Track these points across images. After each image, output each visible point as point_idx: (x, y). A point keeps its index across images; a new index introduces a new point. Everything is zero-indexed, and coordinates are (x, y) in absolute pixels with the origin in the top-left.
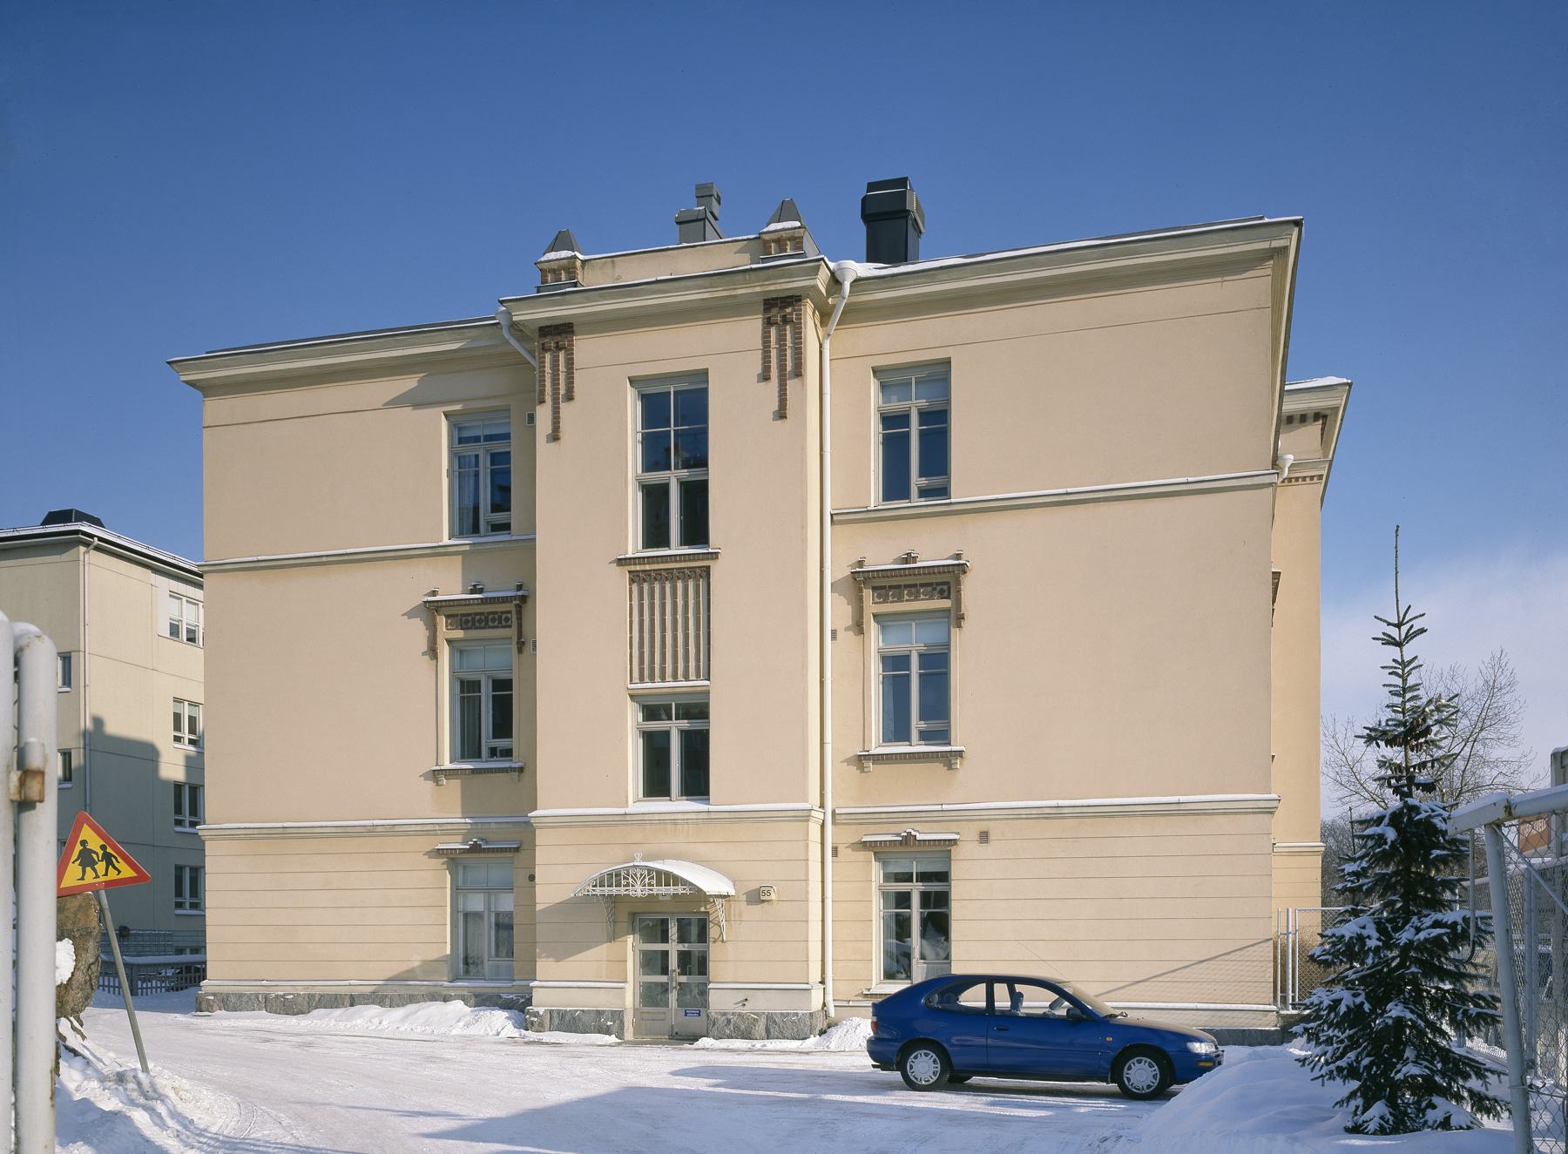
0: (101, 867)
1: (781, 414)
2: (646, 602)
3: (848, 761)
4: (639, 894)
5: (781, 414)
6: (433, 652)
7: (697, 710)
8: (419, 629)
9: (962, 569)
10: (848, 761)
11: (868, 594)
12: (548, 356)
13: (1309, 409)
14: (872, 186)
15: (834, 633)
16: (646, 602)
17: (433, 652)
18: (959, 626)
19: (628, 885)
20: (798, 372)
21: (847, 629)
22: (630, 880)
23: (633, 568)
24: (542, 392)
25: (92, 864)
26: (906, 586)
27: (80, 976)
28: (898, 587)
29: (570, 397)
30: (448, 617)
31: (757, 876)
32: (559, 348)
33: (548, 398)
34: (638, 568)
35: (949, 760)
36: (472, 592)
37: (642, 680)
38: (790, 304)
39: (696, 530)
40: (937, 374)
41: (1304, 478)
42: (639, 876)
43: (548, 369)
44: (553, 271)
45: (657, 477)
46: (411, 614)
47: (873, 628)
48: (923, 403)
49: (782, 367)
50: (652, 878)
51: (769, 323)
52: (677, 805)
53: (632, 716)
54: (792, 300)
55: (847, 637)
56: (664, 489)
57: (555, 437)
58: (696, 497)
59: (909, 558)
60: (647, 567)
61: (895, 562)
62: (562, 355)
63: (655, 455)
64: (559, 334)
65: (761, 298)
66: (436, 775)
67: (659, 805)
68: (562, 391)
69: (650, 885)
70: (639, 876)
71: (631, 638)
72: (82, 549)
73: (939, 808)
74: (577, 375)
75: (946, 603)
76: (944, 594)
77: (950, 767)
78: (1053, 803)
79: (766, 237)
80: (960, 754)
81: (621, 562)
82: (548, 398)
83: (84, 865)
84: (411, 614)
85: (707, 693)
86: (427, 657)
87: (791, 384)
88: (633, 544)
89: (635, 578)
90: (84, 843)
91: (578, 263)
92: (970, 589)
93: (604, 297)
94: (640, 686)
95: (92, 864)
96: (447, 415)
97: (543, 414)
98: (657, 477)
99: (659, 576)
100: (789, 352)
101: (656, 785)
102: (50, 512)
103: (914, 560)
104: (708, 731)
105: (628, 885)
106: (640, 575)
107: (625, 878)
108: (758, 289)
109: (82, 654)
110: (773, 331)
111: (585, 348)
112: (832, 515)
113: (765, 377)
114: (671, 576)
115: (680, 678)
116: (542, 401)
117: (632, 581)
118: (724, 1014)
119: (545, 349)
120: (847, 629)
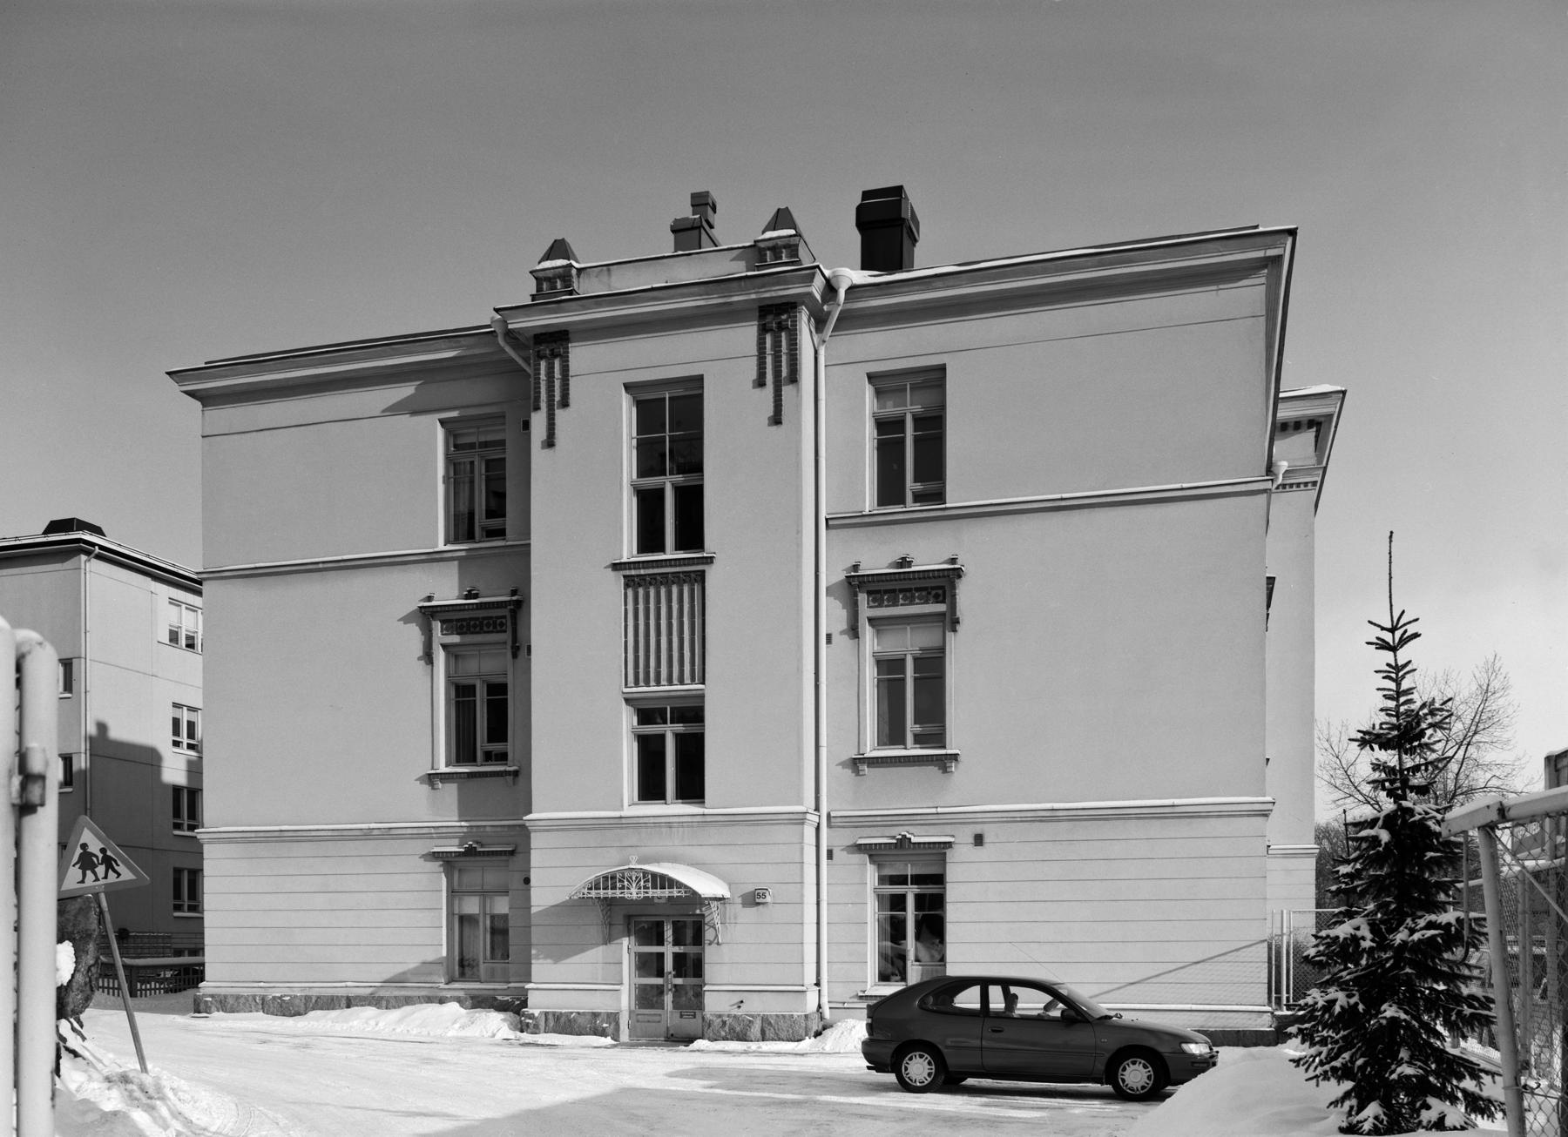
0: (101, 870)
1: (776, 420)
2: (641, 607)
3: (843, 764)
4: (634, 896)
5: (776, 420)
6: (428, 657)
7: (692, 713)
8: (414, 633)
9: (958, 573)
10: (843, 764)
11: (863, 598)
12: (543, 364)
13: (1304, 416)
14: (867, 195)
15: (829, 637)
16: (641, 607)
17: (428, 657)
18: (954, 631)
19: (623, 888)
20: (794, 378)
21: (842, 633)
22: (626, 883)
23: (628, 573)
24: (537, 399)
25: (93, 867)
26: (901, 591)
27: (80, 978)
28: (894, 591)
29: (565, 404)
30: (443, 622)
31: (753, 878)
32: (554, 355)
33: (543, 405)
34: (633, 572)
35: (944, 763)
36: (467, 597)
37: (637, 684)
38: (785, 311)
39: (692, 535)
40: (933, 378)
41: (1298, 485)
42: (634, 878)
43: (543, 376)
44: (548, 279)
45: (651, 482)
46: (406, 619)
47: (867, 632)
48: (917, 408)
49: (777, 373)
50: (648, 881)
51: (763, 330)
52: (673, 808)
53: (627, 720)
54: (789, 307)
55: (842, 641)
56: (659, 494)
57: (550, 443)
58: (691, 503)
59: (904, 562)
60: (642, 572)
61: (890, 566)
62: (557, 363)
63: (650, 461)
64: (554, 342)
65: (756, 306)
66: (432, 779)
67: (654, 809)
68: (557, 398)
69: (645, 887)
70: (634, 878)
71: (626, 642)
72: (83, 557)
73: (934, 811)
74: (572, 382)
75: (942, 608)
76: (939, 599)
77: (945, 770)
78: (1049, 806)
79: (762, 245)
80: (955, 757)
81: (616, 567)
82: (543, 405)
83: (84, 869)
84: (406, 619)
85: (702, 697)
86: (422, 662)
87: (787, 391)
88: (628, 549)
89: (630, 582)
90: (84, 846)
91: (574, 272)
92: (966, 594)
93: (599, 305)
94: (635, 690)
95: (93, 867)
96: (442, 422)
97: (538, 421)
98: (651, 482)
99: (654, 581)
100: (784, 358)
101: (651, 789)
102: (51, 522)
103: (909, 564)
104: (702, 735)
105: (623, 888)
106: (635, 579)
107: (620, 881)
108: (753, 296)
109: (83, 660)
110: (769, 339)
111: (580, 355)
112: (827, 520)
113: (760, 383)
114: (666, 580)
115: (675, 682)
116: (537, 408)
117: (627, 586)
118: (720, 1016)
119: (540, 357)
120: (842, 633)
